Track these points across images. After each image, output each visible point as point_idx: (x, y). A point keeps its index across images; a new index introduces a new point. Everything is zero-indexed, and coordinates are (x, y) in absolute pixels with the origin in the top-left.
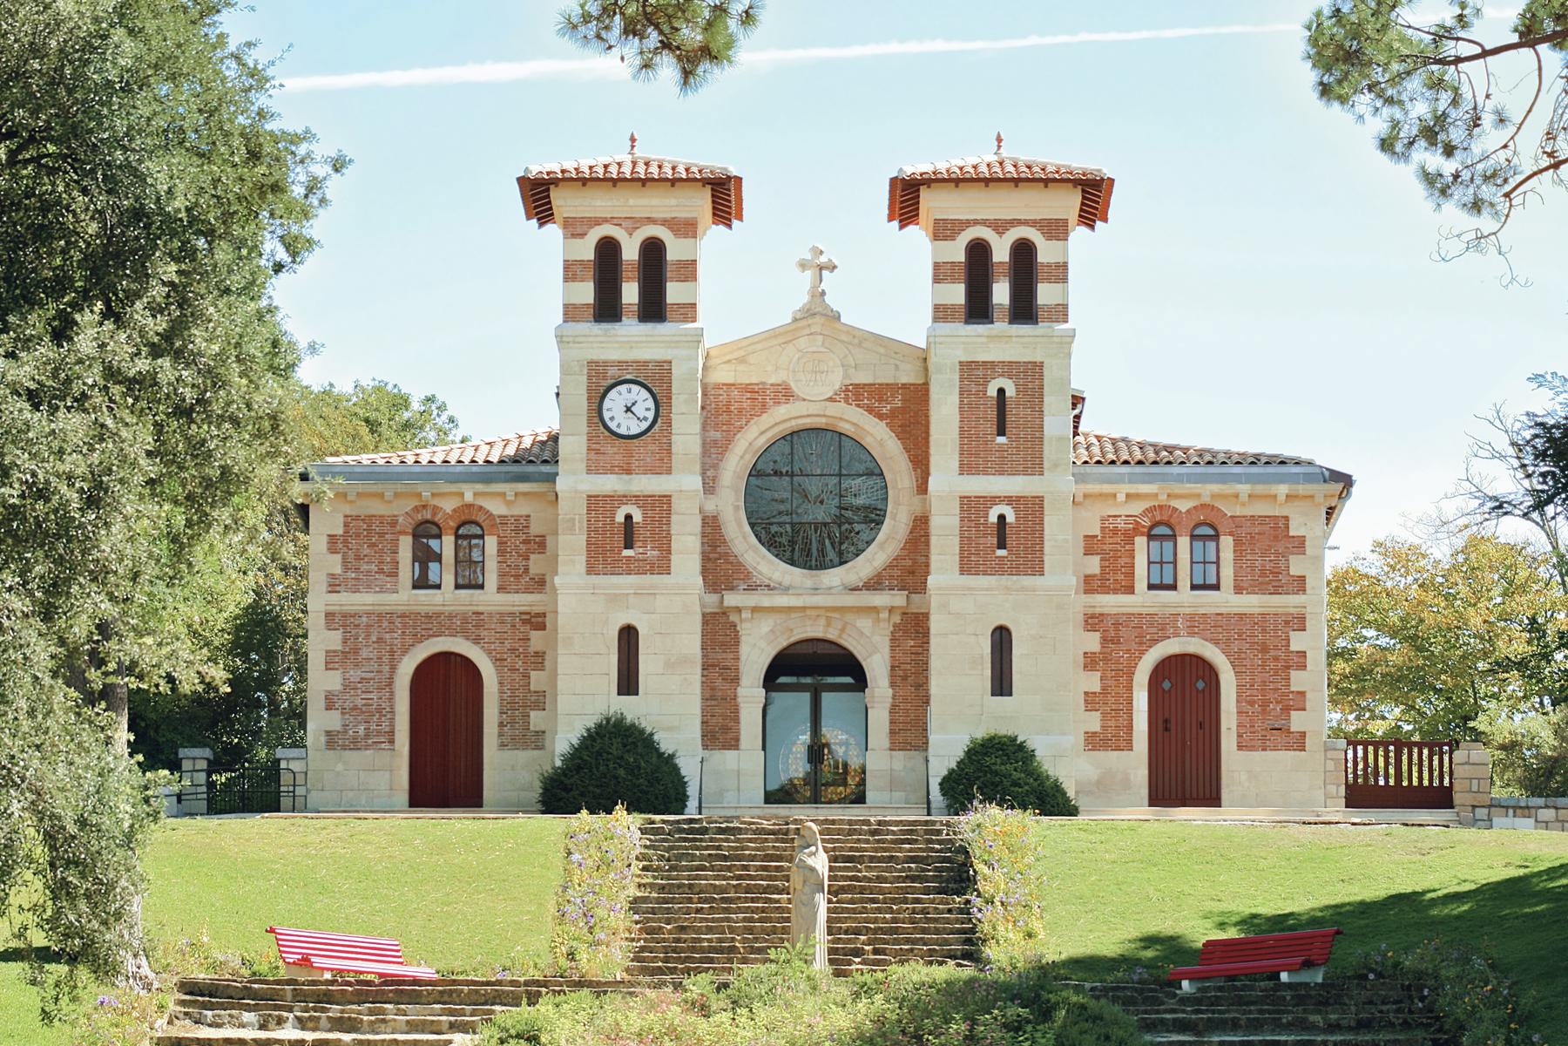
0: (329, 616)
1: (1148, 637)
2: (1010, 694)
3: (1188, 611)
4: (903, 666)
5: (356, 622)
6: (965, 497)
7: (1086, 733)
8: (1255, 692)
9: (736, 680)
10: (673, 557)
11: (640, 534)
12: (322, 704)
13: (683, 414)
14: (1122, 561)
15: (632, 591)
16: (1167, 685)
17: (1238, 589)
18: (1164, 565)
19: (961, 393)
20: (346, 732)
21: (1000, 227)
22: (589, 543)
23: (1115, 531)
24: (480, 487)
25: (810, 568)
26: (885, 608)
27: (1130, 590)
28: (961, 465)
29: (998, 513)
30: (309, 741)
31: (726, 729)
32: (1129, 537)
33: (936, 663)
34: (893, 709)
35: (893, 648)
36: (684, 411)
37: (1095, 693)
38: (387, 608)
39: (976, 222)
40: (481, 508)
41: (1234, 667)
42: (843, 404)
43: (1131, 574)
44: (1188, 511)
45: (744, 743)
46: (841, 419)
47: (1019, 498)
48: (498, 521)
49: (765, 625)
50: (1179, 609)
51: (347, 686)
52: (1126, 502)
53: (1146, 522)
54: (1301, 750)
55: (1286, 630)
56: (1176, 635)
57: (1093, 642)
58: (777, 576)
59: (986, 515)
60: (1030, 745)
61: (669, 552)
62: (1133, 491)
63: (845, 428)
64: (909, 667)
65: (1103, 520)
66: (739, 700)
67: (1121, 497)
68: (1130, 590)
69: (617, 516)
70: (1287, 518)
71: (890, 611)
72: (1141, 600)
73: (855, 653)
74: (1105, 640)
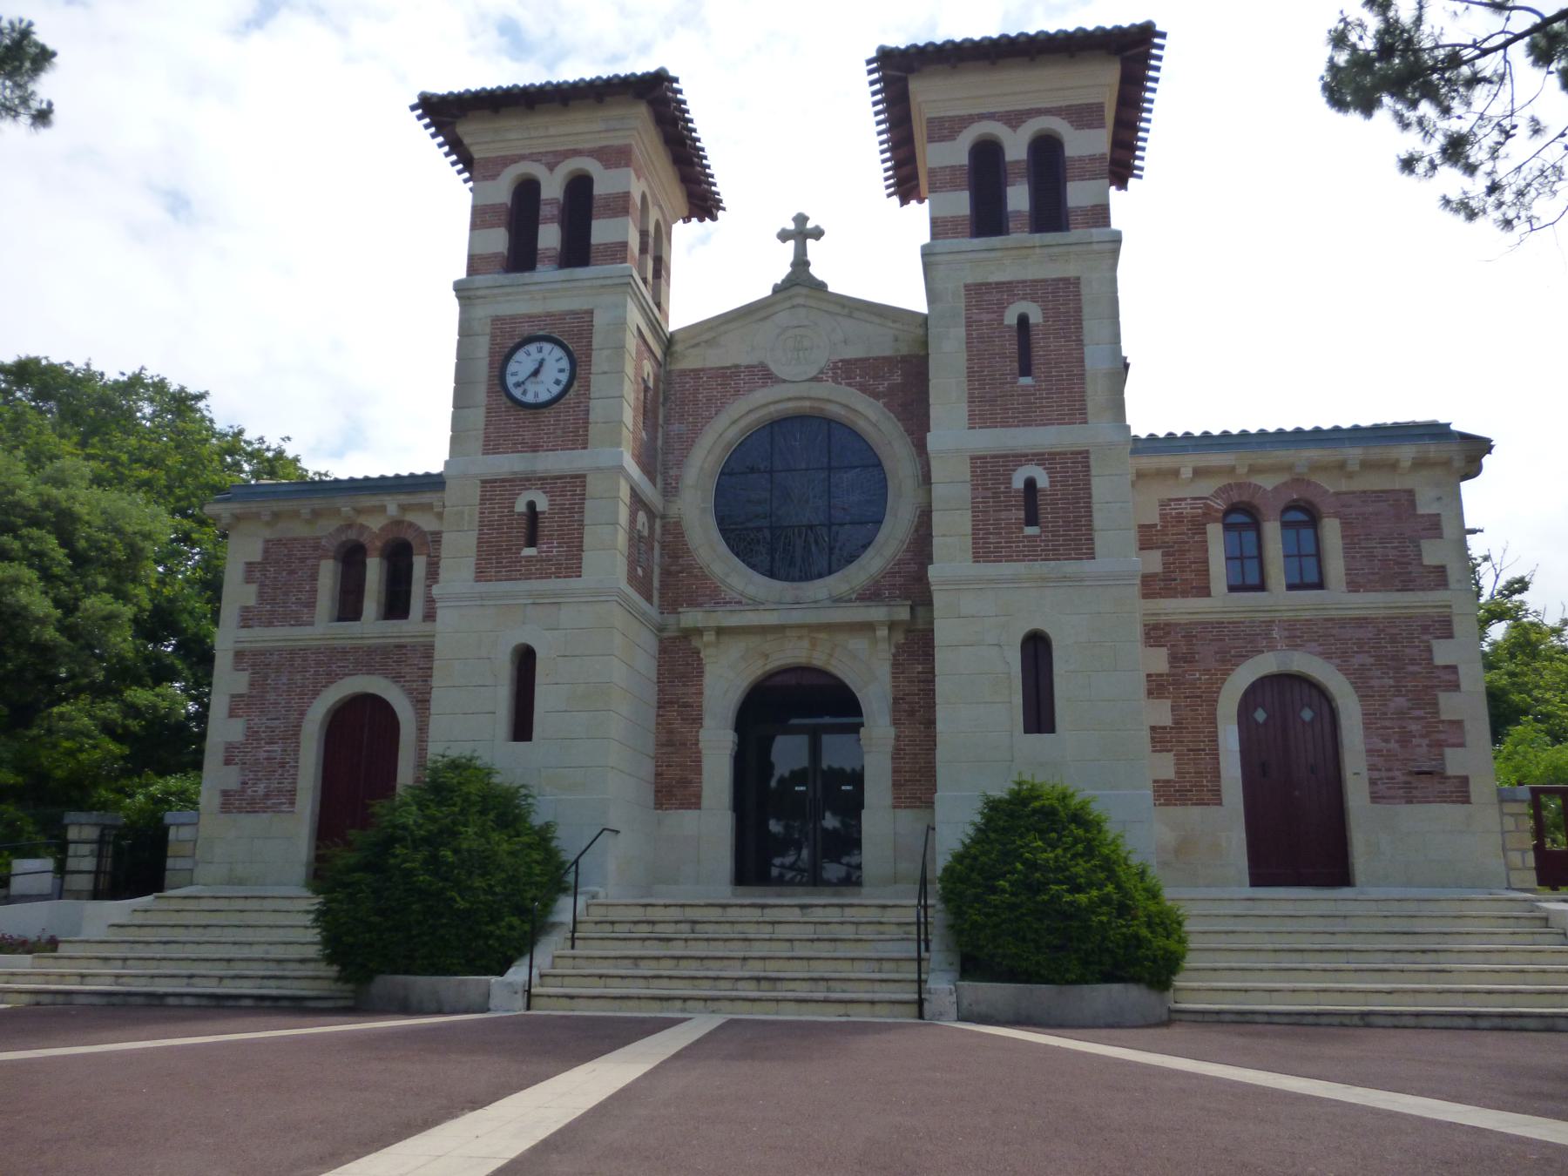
0: (239, 655)
1: (1233, 652)
2: (1052, 730)
3: (1286, 615)
4: (908, 699)
5: (267, 661)
6: (979, 458)
7: (1155, 781)
8: (1387, 723)
9: (697, 721)
10: (584, 555)
11: (545, 526)
12: (221, 757)
13: (605, 373)
14: (1191, 556)
15: (530, 601)
16: (1260, 716)
17: (1353, 586)
18: (1245, 561)
19: (969, 325)
20: (243, 791)
21: (1014, 119)
22: (480, 542)
23: (1179, 518)
24: (404, 499)
25: (793, 580)
26: (882, 623)
27: (1205, 591)
28: (971, 416)
29: (1022, 311)
30: (203, 800)
31: (685, 783)
32: (1199, 526)
33: (942, 687)
34: (897, 754)
35: (895, 677)
36: (606, 369)
37: (1164, 728)
38: (300, 643)
39: (982, 117)
40: (411, 525)
41: (1357, 689)
42: (830, 384)
43: (1204, 572)
44: (1276, 489)
45: (706, 802)
46: (829, 401)
47: (1053, 456)
48: (429, 538)
49: (735, 649)
50: (1273, 614)
51: (252, 734)
52: (1192, 480)
53: (1220, 505)
54: (1463, 803)
55: (1425, 637)
56: (1272, 648)
57: (1159, 660)
58: (751, 591)
59: (1009, 481)
60: (1096, 809)
61: (580, 548)
62: (1202, 464)
63: (833, 410)
64: (916, 699)
65: (1164, 504)
66: (701, 745)
67: (1187, 473)
68: (1205, 591)
69: (516, 505)
70: (1411, 493)
71: (890, 629)
72: (1220, 603)
73: (847, 681)
74: (1174, 659)
